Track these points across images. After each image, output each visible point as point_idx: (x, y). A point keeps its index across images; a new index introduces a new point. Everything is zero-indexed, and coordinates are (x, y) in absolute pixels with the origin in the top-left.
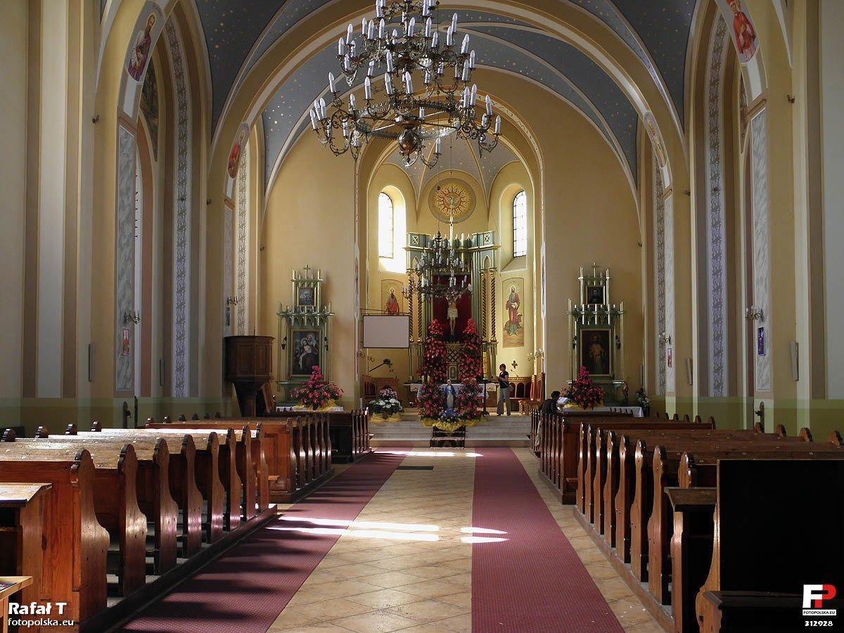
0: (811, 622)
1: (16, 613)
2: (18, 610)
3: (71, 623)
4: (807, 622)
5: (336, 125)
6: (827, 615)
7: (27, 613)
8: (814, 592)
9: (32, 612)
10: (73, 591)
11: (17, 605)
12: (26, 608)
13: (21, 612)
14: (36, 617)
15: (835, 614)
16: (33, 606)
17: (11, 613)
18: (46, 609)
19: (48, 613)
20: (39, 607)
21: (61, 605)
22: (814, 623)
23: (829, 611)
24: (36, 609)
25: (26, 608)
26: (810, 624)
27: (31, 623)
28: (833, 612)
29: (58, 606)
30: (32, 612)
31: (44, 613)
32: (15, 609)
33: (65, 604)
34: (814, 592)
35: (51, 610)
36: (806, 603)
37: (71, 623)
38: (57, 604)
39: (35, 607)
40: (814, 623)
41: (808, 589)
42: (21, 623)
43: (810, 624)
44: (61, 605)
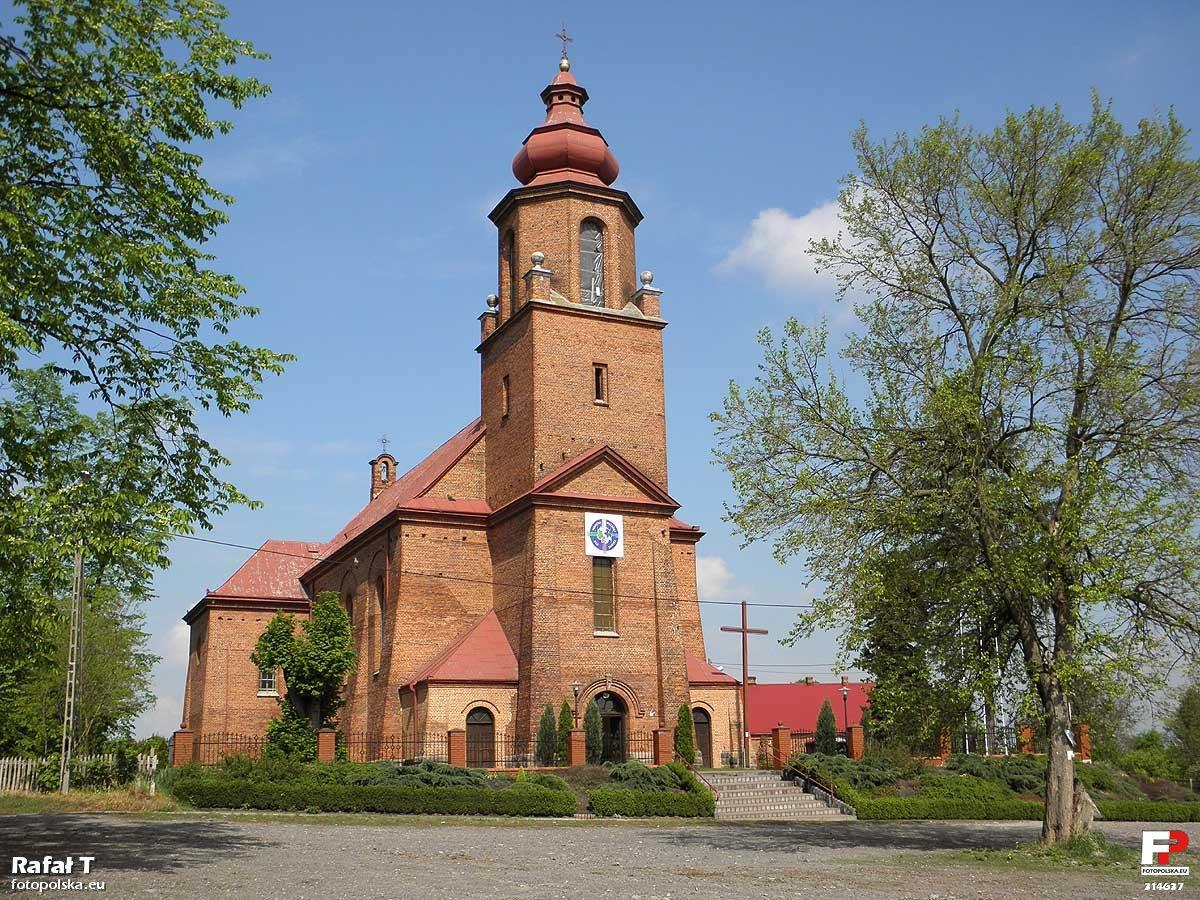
1: (23, 871)
2: (26, 867)
7: (38, 871)
8: (1156, 842)
9: (46, 871)
11: (24, 861)
12: (37, 864)
15: (1187, 874)
16: (47, 861)
19: (69, 871)
20: (55, 863)
21: (87, 860)
23: (1179, 869)
24: (51, 866)
25: (37, 864)
27: (44, 885)
30: (46, 871)
32: (22, 866)
33: (93, 859)
34: (1156, 842)
36: (1147, 858)
39: (50, 863)
42: (29, 886)
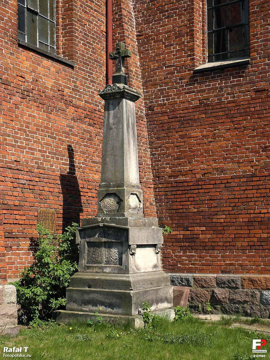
0: (256, 355)
2: (8, 350)
3: (30, 356)
4: (254, 355)
5: (79, 201)
6: (263, 352)
7: (11, 351)
8: (257, 343)
10: (5, 238)
12: (11, 349)
13: (9, 351)
14: (15, 353)
17: (4, 351)
18: (19, 350)
19: (21, 351)
20: (17, 349)
21: (26, 348)
22: (257, 356)
24: (15, 350)
25: (11, 349)
26: (255, 356)
28: (265, 351)
29: (25, 349)
30: (14, 351)
31: (19, 351)
34: (257, 343)
35: (22, 350)
36: (254, 347)
37: (30, 356)
38: (24, 348)
39: (15, 349)
40: (257, 356)
41: (255, 341)
42: (9, 355)
43: (255, 356)
44: (26, 348)
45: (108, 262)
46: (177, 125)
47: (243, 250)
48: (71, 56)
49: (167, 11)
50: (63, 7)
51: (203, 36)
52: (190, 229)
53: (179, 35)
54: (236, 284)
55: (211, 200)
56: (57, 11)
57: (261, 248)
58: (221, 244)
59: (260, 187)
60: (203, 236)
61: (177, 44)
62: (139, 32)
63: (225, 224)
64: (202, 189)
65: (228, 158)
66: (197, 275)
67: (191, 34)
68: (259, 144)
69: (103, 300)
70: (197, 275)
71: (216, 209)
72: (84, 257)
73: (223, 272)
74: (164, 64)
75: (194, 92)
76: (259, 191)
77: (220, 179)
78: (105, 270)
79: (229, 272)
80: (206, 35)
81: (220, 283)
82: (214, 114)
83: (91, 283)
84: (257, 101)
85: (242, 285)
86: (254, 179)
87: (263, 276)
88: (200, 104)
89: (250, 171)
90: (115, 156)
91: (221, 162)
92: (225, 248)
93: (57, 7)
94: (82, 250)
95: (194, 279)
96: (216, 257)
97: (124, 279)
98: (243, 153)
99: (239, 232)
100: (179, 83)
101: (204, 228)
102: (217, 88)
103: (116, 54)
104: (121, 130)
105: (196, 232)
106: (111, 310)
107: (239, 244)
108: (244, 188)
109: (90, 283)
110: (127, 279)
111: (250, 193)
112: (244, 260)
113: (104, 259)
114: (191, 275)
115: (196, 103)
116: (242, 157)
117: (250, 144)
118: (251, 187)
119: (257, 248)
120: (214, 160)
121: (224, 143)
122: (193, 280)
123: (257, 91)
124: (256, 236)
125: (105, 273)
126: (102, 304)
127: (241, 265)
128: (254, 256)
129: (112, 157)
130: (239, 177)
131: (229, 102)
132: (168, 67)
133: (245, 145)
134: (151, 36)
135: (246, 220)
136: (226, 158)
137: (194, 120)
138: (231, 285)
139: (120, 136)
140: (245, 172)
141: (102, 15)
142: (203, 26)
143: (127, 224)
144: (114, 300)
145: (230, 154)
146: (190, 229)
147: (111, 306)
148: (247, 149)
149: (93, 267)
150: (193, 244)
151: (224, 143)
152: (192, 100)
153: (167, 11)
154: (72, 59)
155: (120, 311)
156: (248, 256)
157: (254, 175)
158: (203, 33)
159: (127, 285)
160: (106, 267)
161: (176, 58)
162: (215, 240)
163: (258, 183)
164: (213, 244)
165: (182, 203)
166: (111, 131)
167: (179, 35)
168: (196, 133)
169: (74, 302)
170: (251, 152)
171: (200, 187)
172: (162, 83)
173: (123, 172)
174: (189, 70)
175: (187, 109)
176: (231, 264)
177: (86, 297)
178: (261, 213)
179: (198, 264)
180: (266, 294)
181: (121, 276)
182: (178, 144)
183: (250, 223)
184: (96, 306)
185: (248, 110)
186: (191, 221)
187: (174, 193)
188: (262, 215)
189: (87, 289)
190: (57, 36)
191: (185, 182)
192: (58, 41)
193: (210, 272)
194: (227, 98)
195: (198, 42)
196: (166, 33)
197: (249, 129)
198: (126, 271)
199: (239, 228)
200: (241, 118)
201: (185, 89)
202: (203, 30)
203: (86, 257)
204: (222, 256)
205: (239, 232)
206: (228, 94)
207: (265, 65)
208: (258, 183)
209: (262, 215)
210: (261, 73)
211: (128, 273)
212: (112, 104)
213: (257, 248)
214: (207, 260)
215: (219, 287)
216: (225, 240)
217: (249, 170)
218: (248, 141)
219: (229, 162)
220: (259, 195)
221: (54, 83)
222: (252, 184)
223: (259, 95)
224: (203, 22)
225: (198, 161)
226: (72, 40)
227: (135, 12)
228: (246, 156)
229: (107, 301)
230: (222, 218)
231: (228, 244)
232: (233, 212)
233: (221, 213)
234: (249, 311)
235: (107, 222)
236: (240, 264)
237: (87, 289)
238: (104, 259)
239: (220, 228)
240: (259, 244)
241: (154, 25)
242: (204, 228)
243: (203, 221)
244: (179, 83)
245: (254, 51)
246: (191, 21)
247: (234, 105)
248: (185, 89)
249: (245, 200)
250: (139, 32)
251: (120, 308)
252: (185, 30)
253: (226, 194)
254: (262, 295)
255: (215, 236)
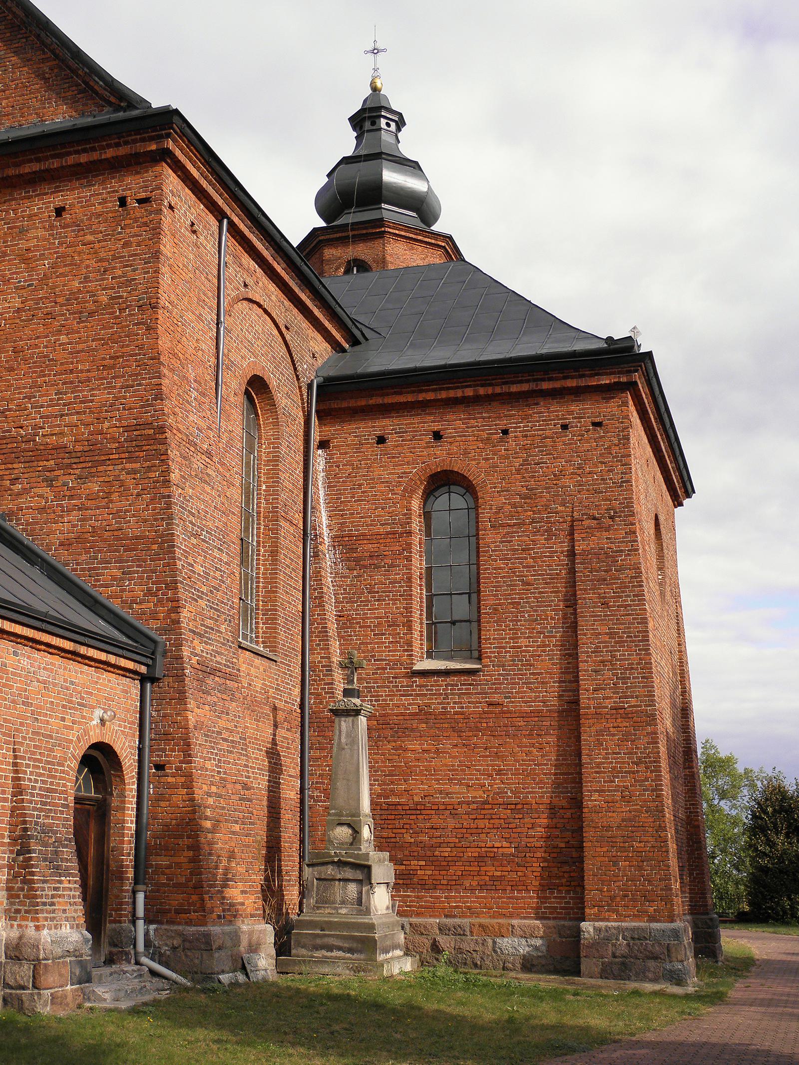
45: (343, 902)
46: (389, 733)
47: (473, 890)
48: (273, 649)
49: (378, 592)
50: (264, 587)
51: (421, 627)
52: (404, 862)
53: (394, 624)
54: (464, 930)
55: (432, 828)
56: (257, 592)
57: (494, 887)
58: (445, 882)
59: (494, 817)
60: (422, 872)
61: (389, 634)
62: (339, 611)
63: (450, 859)
64: (421, 814)
65: (455, 779)
66: (414, 920)
67: (409, 625)
68: (492, 765)
69: (341, 944)
70: (414, 920)
71: (439, 840)
72: (312, 895)
73: (446, 916)
74: (373, 656)
75: (411, 695)
76: (492, 821)
77: (444, 803)
78: (339, 911)
79: (455, 916)
80: (425, 626)
81: (442, 929)
82: (438, 726)
83: (324, 926)
84: (490, 716)
85: (471, 932)
86: (486, 806)
87: (496, 921)
88: (420, 711)
89: (481, 797)
90: (348, 780)
91: (446, 784)
92: (449, 887)
93: (258, 587)
94: (310, 887)
95: (411, 924)
96: (437, 898)
97: (367, 921)
98: (474, 775)
99: (467, 868)
100: (392, 682)
101: (423, 863)
102: (441, 694)
103: (348, 663)
104: (356, 752)
105: (413, 867)
106: (351, 956)
107: (467, 883)
108: (474, 817)
109: (323, 926)
110: (371, 922)
111: (481, 823)
112: (472, 901)
113: (338, 899)
114: (407, 920)
115: (414, 709)
116: (472, 779)
117: (481, 765)
118: (482, 816)
119: (489, 887)
120: (438, 780)
121: (449, 761)
122: (409, 926)
123: (490, 704)
124: (488, 874)
125: (340, 914)
126: (340, 949)
127: (469, 908)
128: (484, 897)
129: (345, 782)
130: (468, 803)
131: (456, 713)
132: (378, 660)
133: (475, 765)
134: (356, 619)
135: (476, 854)
136: (452, 779)
137: (413, 730)
138: (458, 931)
139: (355, 758)
140: (476, 797)
141: (299, 591)
142: (421, 615)
143: (368, 860)
144: (355, 945)
145: (457, 775)
146: (404, 862)
147: (350, 950)
148: (478, 770)
149: (324, 907)
150: (408, 882)
151: (449, 761)
152: (409, 704)
153: (378, 592)
154: (275, 651)
155: (362, 956)
156: (477, 897)
157: (486, 802)
158: (421, 623)
159: (371, 927)
160: (341, 908)
161: (389, 651)
162: (437, 877)
163: (491, 812)
164: (434, 882)
165: (395, 831)
166: (343, 752)
167: (394, 624)
168: (414, 745)
169: (302, 947)
170: (483, 774)
171: (418, 812)
172: (370, 678)
173: (359, 800)
174: (405, 668)
175: (402, 714)
176: (457, 907)
177: (319, 941)
178: (494, 847)
179: (415, 906)
180: (500, 941)
181: (361, 918)
182: (390, 757)
183: (480, 859)
184: (332, 951)
185: (479, 725)
186: (407, 853)
187: (383, 817)
188: (496, 850)
189: (320, 932)
190: (257, 623)
191: (399, 804)
192: (257, 628)
193: (431, 916)
194: (454, 708)
195: (416, 635)
196: (377, 618)
197: (481, 747)
198: (368, 912)
199: (468, 864)
200: (471, 734)
201: (400, 691)
202: (421, 619)
203: (314, 896)
204: (446, 897)
205: (467, 868)
206: (455, 703)
207: (499, 675)
208: (491, 812)
209: (496, 850)
210: (494, 684)
211: (370, 915)
212: (345, 721)
213: (489, 887)
214: (426, 902)
215: (442, 934)
216: (449, 878)
217: (480, 795)
218: (479, 761)
219: (455, 784)
220: (491, 826)
221: (263, 684)
222: (483, 812)
223: (491, 709)
224: (421, 610)
225: (415, 780)
226: (275, 628)
227: (333, 586)
228: (477, 779)
229: (346, 945)
230: (446, 852)
231: (454, 883)
232: (460, 845)
233: (445, 845)
234: (479, 963)
235: (343, 856)
236: (468, 906)
237: (320, 932)
238: (338, 899)
239: (445, 863)
240: (491, 883)
241: (359, 606)
242: (423, 863)
243: (422, 853)
244: (392, 682)
245: (487, 657)
246: (408, 609)
247: (463, 716)
248: (400, 691)
249: (474, 831)
250: (339, 611)
251: (361, 953)
252: (401, 619)
253: (451, 823)
254: (494, 943)
255: (437, 872)
